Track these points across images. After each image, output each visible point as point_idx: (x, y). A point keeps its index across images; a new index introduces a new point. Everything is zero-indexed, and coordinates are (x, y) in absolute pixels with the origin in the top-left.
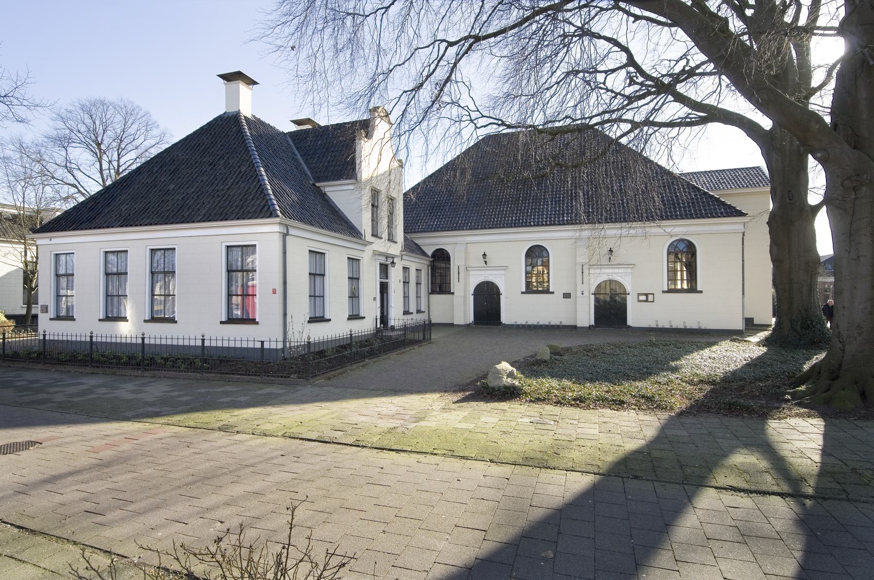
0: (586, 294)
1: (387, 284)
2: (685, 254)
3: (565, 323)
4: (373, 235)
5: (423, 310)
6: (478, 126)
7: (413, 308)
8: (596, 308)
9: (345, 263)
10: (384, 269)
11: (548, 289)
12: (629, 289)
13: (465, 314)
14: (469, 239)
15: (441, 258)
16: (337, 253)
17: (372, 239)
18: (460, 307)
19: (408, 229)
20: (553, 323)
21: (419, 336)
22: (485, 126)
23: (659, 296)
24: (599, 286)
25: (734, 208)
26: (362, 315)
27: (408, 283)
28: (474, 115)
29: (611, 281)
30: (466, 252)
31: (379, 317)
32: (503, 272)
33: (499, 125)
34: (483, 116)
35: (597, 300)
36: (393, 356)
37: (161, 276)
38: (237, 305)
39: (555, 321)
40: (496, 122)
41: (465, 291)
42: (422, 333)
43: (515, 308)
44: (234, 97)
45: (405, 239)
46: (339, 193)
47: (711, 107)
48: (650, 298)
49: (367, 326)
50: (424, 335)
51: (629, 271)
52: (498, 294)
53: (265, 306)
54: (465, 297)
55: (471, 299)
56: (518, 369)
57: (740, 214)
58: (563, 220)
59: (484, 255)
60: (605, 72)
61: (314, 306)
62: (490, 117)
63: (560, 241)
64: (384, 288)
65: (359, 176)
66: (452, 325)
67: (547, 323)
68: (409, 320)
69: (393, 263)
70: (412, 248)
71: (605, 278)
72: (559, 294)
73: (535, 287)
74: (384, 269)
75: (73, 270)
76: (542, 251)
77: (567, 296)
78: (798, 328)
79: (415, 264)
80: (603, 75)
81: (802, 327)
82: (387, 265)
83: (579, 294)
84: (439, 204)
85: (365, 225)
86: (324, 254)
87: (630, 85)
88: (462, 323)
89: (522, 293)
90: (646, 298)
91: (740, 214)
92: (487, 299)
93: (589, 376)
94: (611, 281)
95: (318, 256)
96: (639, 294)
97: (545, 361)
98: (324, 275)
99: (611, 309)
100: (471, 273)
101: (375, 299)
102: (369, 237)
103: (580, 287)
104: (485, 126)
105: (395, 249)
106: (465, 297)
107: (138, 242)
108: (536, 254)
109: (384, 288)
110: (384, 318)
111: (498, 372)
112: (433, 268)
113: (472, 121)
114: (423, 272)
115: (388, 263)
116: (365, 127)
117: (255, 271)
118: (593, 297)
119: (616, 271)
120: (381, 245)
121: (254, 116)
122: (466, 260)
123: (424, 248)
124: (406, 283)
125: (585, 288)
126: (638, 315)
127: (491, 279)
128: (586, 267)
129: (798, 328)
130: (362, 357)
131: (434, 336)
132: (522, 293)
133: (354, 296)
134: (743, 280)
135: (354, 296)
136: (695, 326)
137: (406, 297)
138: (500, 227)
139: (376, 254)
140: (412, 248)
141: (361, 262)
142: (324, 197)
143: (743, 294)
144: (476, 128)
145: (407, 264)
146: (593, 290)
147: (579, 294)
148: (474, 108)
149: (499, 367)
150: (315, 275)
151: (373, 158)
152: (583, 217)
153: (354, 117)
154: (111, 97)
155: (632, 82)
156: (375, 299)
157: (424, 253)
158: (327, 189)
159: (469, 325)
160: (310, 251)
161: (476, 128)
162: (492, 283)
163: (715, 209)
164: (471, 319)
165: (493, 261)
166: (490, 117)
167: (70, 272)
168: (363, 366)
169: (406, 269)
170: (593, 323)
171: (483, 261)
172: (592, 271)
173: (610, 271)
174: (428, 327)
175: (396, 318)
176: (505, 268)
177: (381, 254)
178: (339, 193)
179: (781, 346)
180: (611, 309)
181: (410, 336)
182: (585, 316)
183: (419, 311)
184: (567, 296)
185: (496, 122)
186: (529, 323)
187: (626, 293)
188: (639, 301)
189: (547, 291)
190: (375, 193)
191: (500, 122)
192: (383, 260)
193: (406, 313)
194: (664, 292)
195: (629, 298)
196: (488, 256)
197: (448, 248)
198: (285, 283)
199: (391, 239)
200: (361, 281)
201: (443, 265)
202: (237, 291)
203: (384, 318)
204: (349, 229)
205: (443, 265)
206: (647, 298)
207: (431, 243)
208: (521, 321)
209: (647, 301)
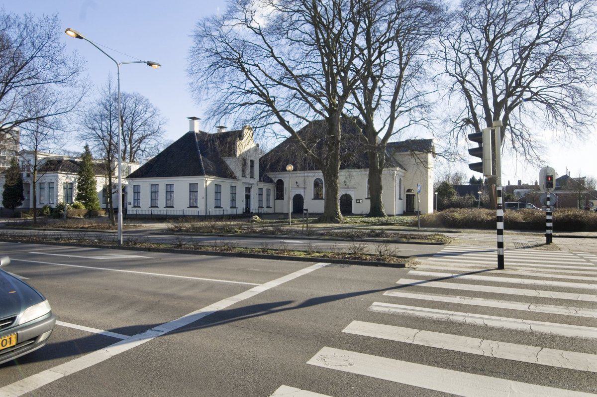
7: (264, 204)
9: (229, 188)
10: (248, 190)
12: (353, 197)
14: (49, 175)
15: (280, 185)
16: (226, 184)
23: (364, 200)
37: (169, 193)
38: (67, 178)
44: (192, 125)
48: (361, 201)
53: (201, 203)
61: (216, 203)
64: (248, 197)
74: (248, 190)
75: (173, 204)
79: (265, 186)
85: (238, 172)
89: (312, 199)
92: (298, 200)
96: (357, 200)
101: (243, 201)
102: (240, 177)
107: (162, 182)
109: (248, 197)
114: (271, 190)
120: (248, 180)
121: (200, 131)
124: (260, 195)
132: (312, 199)
133: (233, 200)
135: (233, 200)
137: (260, 201)
151: (244, 146)
154: (151, 101)
172: (292, 190)
176: (354, 188)
177: (245, 183)
183: (268, 207)
188: (357, 203)
192: (247, 186)
193: (259, 207)
198: (206, 195)
199: (252, 177)
207: (276, 177)
209: (359, 203)
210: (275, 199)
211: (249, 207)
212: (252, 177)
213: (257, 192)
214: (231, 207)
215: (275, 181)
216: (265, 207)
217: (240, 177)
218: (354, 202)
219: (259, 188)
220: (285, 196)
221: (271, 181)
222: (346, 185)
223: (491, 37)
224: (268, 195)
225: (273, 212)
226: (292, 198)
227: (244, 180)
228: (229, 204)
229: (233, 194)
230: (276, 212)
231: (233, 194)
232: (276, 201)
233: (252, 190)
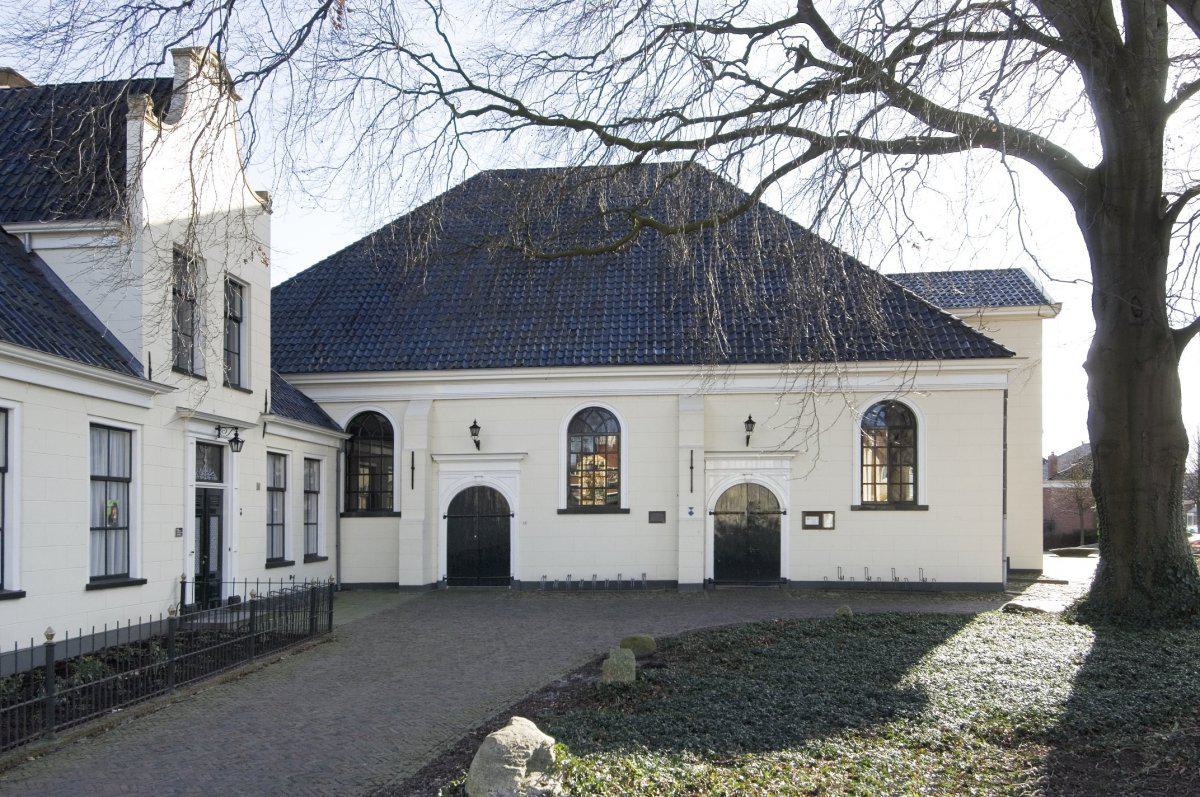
0: (698, 513)
1: (219, 495)
2: (894, 432)
3: (652, 576)
4: (177, 369)
5: (322, 553)
6: (461, 111)
7: (294, 550)
8: (718, 543)
10: (211, 458)
11: (617, 503)
12: (785, 502)
13: (427, 556)
14: (440, 390)
15: (369, 436)
17: (173, 379)
18: (413, 546)
19: (282, 361)
20: (626, 577)
21: (300, 621)
22: (477, 113)
24: (724, 497)
25: (990, 341)
26: (136, 574)
27: (283, 490)
28: (450, 81)
29: (749, 486)
30: (431, 420)
31: (191, 577)
32: (516, 466)
33: (512, 113)
34: (472, 87)
35: (720, 527)
36: (209, 689)
39: (631, 574)
40: (507, 105)
41: (428, 509)
42: (304, 617)
43: (546, 546)
45: (276, 384)
46: (67, 255)
47: (970, 121)
48: (828, 521)
49: (153, 601)
50: (313, 621)
51: (787, 464)
52: (506, 515)
54: (427, 525)
55: (443, 527)
56: (559, 737)
57: (1001, 353)
58: (651, 355)
59: (475, 428)
60: (750, 32)
62: (489, 91)
63: (646, 401)
64: (209, 506)
65: (134, 219)
66: (394, 587)
67: (613, 577)
68: (276, 582)
69: (236, 440)
70: (290, 404)
71: (737, 479)
72: (640, 515)
73: (594, 495)
74: (211, 458)
76: (604, 421)
77: (657, 517)
78: (1148, 584)
79: (298, 443)
80: (745, 39)
81: (1154, 582)
82: (221, 448)
83: (684, 514)
84: (358, 313)
85: (154, 348)
86: (285, 456)
87: (797, 68)
88: (419, 581)
89: (561, 512)
90: (814, 520)
91: (1001, 353)
92: (479, 529)
93: (743, 732)
94: (749, 486)
95: (115, 439)
97: (625, 688)
98: (128, 481)
99: (748, 546)
100: (443, 467)
101: (179, 532)
102: (163, 373)
103: (686, 500)
104: (477, 113)
105: (249, 407)
106: (427, 525)
108: (591, 427)
109: (209, 506)
110: (208, 582)
111: (502, 755)
112: (352, 459)
113: (442, 94)
114: (323, 466)
115: (223, 440)
116: (163, 96)
117: (269, 489)
118: (711, 520)
119: (761, 464)
122: (430, 437)
123: (328, 410)
124: (276, 490)
125: (695, 500)
126: (802, 558)
127: (488, 481)
128: (699, 457)
129: (1148, 584)
130: (101, 699)
131: (343, 616)
132: (561, 512)
133: (111, 525)
134: (1005, 486)
135: (111, 525)
136: (915, 578)
137: (276, 525)
138: (513, 366)
139: (184, 416)
140: (290, 404)
141: (137, 438)
142: (29, 266)
143: (1004, 512)
144: (456, 115)
145: (279, 445)
146: (711, 507)
147: (684, 514)
148: (448, 63)
149: (503, 736)
150: (107, 479)
151: (173, 175)
152: (719, 335)
153: (121, 68)
155: (803, 57)
156: (179, 532)
157: (327, 422)
158: (38, 243)
159: (435, 586)
160: (93, 425)
161: (456, 115)
162: (493, 492)
163: (954, 342)
164: (440, 571)
165: (492, 441)
166: (489, 91)
167: (101, 485)
168: (91, 735)
169: (276, 457)
170: (710, 574)
171: (470, 440)
172: (710, 465)
173: (752, 464)
174: (321, 599)
175: (245, 573)
177: (201, 418)
178: (67, 255)
179: (1113, 622)
180: (748, 546)
181: (277, 623)
182: (696, 563)
183: (310, 558)
184: (657, 517)
185: (507, 105)
186: (575, 578)
187: (778, 511)
188: (806, 527)
189: (613, 507)
190: (183, 261)
191: (516, 108)
192: (207, 433)
193: (273, 563)
194: (854, 508)
195: (785, 521)
196: (480, 427)
197: (389, 412)
199: (233, 382)
200: (135, 487)
201: (377, 451)
202: (881, 470)
203: (208, 582)
204: (101, 351)
205: (377, 451)
206: (821, 521)
207: (345, 397)
208: (557, 574)
209: (820, 526)
210: (342, 515)
211: (213, 567)
212: (233, 382)
213: (262, 473)
214: (97, 584)
215: (343, 417)
216: (299, 558)
217: (163, 373)
218: (789, 528)
219: (305, 459)
220: (404, 496)
221: (316, 416)
222: (478, 444)
223: (428, 154)
224: (310, 492)
225: (103, 573)
226: (444, 510)
227: (186, 392)
228: (81, 557)
229: (112, 481)
230: (348, 578)
231: (112, 481)
232: (345, 521)
233: (233, 462)
